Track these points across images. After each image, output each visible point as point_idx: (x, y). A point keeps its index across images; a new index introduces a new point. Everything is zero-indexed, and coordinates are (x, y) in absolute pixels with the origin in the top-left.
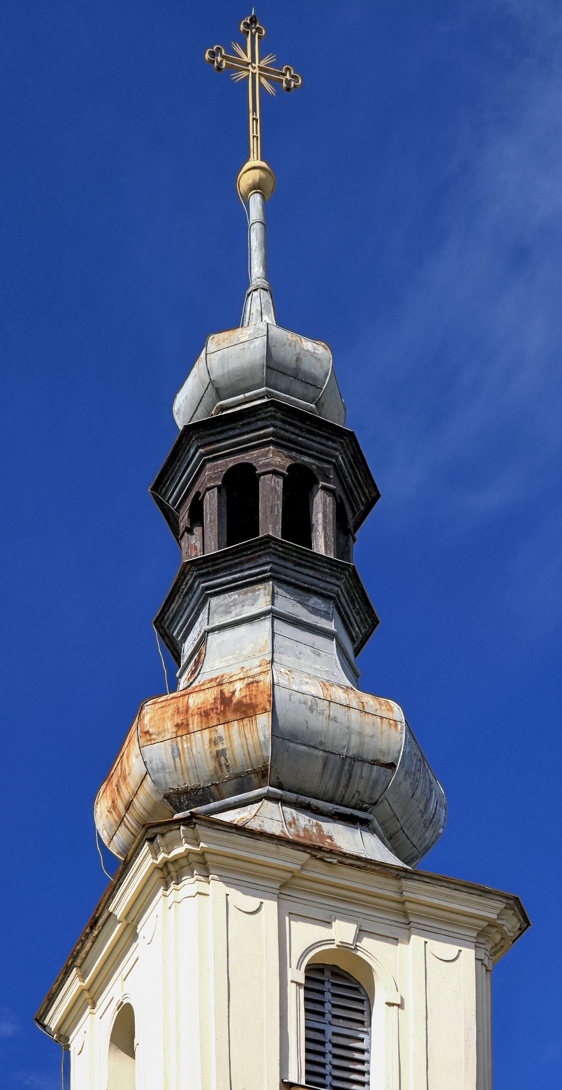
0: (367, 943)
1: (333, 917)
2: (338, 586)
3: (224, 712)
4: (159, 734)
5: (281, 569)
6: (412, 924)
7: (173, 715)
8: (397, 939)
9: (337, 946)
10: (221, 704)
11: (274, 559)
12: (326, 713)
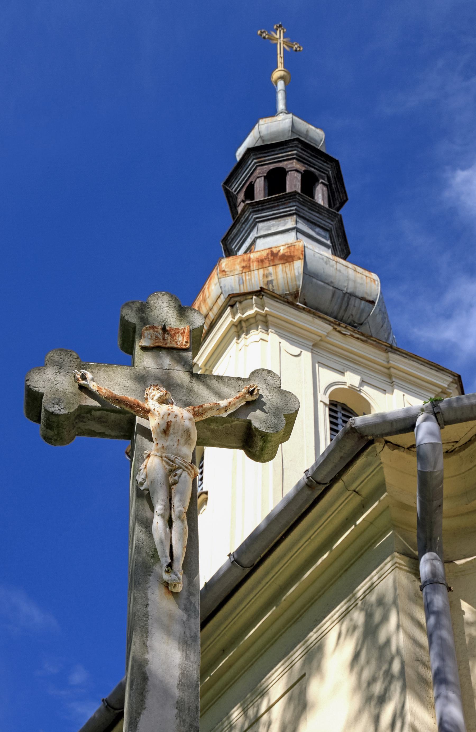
0: (366, 389)
1: (345, 370)
2: (331, 225)
3: (273, 260)
4: (231, 271)
5: (301, 210)
6: (394, 383)
7: (240, 262)
8: (385, 391)
9: (349, 387)
10: (271, 256)
11: (297, 204)
12: (335, 266)
